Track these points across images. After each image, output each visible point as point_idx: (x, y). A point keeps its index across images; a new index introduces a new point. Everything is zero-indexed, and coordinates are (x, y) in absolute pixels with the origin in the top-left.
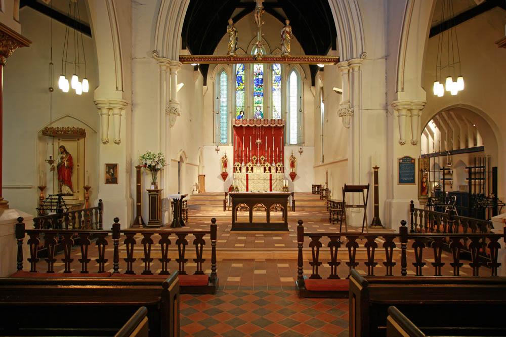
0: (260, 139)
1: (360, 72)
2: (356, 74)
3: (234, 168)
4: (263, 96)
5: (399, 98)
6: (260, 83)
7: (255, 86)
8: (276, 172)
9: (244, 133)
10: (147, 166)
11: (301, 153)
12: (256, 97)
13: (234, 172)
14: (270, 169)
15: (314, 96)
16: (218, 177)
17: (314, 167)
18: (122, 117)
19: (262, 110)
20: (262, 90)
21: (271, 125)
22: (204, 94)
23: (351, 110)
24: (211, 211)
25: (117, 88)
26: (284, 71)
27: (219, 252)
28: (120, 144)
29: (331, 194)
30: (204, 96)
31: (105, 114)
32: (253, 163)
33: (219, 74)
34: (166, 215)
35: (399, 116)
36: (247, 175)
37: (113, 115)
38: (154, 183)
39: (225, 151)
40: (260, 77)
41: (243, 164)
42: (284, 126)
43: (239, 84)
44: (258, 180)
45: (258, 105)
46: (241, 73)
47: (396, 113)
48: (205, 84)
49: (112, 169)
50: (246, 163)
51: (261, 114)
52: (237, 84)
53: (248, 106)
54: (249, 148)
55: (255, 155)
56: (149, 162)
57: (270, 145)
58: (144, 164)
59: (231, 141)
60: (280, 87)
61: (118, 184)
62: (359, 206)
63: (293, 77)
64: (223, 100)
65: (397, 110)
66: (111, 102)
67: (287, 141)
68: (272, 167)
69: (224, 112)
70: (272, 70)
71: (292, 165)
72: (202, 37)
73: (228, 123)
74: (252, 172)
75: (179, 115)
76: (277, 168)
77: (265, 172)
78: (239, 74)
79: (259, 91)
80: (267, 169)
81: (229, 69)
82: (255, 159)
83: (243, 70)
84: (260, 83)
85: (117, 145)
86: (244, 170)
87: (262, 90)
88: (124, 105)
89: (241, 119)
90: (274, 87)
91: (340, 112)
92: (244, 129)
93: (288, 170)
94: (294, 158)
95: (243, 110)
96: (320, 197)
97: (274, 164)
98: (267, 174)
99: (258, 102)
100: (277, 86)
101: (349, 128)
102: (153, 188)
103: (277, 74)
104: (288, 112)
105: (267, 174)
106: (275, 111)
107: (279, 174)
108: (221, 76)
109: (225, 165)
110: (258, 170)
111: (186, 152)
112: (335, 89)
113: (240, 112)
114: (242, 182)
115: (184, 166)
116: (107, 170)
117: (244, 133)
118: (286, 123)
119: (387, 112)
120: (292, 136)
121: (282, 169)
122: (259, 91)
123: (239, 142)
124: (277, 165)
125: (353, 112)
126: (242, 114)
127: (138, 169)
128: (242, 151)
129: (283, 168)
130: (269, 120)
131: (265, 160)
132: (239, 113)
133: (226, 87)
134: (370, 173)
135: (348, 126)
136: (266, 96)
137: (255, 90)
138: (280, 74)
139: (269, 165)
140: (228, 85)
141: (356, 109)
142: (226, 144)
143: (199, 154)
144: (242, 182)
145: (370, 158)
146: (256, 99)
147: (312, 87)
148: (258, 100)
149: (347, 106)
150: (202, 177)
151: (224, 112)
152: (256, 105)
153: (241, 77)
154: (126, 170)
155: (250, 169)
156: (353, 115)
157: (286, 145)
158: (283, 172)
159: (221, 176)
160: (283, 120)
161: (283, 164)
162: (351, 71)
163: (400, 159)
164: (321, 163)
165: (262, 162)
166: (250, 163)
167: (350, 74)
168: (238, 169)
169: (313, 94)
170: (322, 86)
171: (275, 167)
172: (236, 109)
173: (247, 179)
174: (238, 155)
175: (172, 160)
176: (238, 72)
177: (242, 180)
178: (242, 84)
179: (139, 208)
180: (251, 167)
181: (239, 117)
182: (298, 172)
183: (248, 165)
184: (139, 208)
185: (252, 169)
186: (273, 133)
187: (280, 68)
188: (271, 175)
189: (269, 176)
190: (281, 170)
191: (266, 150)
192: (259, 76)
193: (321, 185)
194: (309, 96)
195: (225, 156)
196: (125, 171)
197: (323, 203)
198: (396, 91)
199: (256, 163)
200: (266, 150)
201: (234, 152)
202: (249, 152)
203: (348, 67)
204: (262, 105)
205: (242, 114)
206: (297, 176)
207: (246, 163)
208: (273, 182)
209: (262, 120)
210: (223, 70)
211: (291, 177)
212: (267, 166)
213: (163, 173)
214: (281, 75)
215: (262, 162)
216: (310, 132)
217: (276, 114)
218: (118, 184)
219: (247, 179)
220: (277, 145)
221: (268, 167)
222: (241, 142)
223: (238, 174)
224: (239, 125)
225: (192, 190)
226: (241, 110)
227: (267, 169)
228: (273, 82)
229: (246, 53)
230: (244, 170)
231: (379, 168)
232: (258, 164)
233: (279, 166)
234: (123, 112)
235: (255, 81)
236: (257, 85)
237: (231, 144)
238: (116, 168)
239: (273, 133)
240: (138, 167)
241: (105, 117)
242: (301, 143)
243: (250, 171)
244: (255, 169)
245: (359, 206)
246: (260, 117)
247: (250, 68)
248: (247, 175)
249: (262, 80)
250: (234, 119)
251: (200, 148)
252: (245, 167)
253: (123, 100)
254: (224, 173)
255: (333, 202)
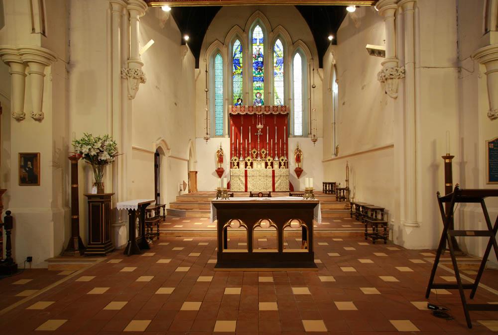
0: (259, 129)
1: (417, 10)
2: (409, 14)
3: (231, 163)
4: (263, 81)
5: (492, 42)
6: (260, 66)
7: (254, 70)
8: (280, 168)
9: (242, 123)
10: (83, 155)
11: (315, 142)
12: (255, 82)
13: (231, 168)
14: (272, 164)
15: (322, 80)
16: (212, 174)
17: (323, 162)
18: (45, 78)
19: (262, 97)
20: (262, 75)
21: (274, 113)
22: (195, 77)
23: (401, 70)
24: (197, 219)
25: (33, 29)
26: (286, 52)
27: (230, 232)
28: (43, 121)
29: (351, 195)
30: (196, 81)
31: (18, 73)
32: (252, 158)
33: (214, 57)
34: (120, 233)
35: (487, 74)
36: (246, 171)
37: (30, 74)
38: (99, 184)
39: (221, 143)
40: (260, 59)
41: (241, 159)
42: (288, 113)
43: (236, 67)
44: (257, 179)
45: (258, 91)
46: (239, 56)
47: (483, 69)
48: (197, 66)
49: (30, 161)
50: (244, 158)
51: (261, 101)
52: (234, 68)
53: (246, 92)
54: (248, 141)
55: (255, 148)
56: (85, 150)
57: (272, 137)
58: (78, 152)
59: (227, 133)
60: (282, 70)
61: (39, 185)
62: (478, 233)
63: (298, 58)
64: (220, 90)
65: (484, 64)
66: (22, 51)
67: (291, 132)
68: (274, 162)
69: (219, 100)
70: (273, 51)
71: (298, 159)
72: (195, 26)
73: (224, 112)
74: (252, 168)
75: (143, 80)
76: (280, 163)
77: (266, 168)
78: (236, 56)
79: (258, 76)
80: (269, 164)
81: (224, 50)
82: (254, 152)
83: (241, 52)
84: (260, 66)
85: (37, 122)
86: (242, 165)
87: (262, 75)
88: (49, 59)
89: (239, 106)
90: (275, 71)
91: (383, 74)
92: (242, 119)
93: (293, 165)
94: (300, 151)
95: (241, 98)
96: (337, 198)
97: (277, 159)
98: (269, 170)
99: (259, 88)
100: (279, 70)
101: (396, 98)
102: (94, 191)
103: (278, 57)
104: (291, 97)
105: (269, 170)
106: (277, 98)
107: (283, 170)
108: (216, 60)
109: (221, 159)
110: (259, 166)
111: (165, 140)
112: (368, 46)
113: (238, 100)
114: (240, 179)
115: (165, 161)
116: (22, 164)
117: (242, 123)
118: (289, 110)
119: (459, 72)
120: (297, 127)
121: (286, 165)
122: (258, 76)
123: (237, 134)
124: (281, 159)
125: (404, 73)
126: (240, 102)
127: (74, 162)
128: (240, 144)
129: (288, 162)
130: (271, 106)
131: (266, 153)
132: (236, 100)
133: (221, 71)
134: (435, 167)
135: (395, 96)
136: (267, 80)
137: (254, 75)
138: (282, 56)
139: (272, 159)
140: (223, 70)
141: (409, 68)
142: (223, 136)
143: (189, 145)
144: (240, 179)
145: (434, 144)
146: (256, 84)
147: (320, 70)
148: (257, 85)
149: (393, 64)
150: (193, 175)
151: (219, 100)
152: (255, 91)
153: (238, 60)
154: (54, 162)
155: (249, 164)
156: (405, 77)
157: (290, 136)
158: (288, 168)
159: (216, 173)
160: (287, 106)
161: (287, 158)
162: (400, 10)
163: (489, 143)
164: (333, 157)
165: (263, 156)
166: (249, 158)
167: (399, 17)
168: (236, 164)
169: (321, 77)
170: (334, 62)
171: (278, 162)
172: (233, 96)
173: (246, 176)
174: (235, 148)
175: (134, 148)
176: (235, 54)
177: (240, 177)
178: (239, 68)
179: (75, 224)
180: (250, 161)
181: (236, 105)
182: (305, 168)
183: (247, 159)
184: (75, 224)
185: (252, 164)
186: (275, 123)
187: (282, 49)
188: (273, 172)
189: (271, 172)
190: (284, 165)
191: (268, 142)
192: (259, 59)
193: (335, 183)
194: (317, 80)
195: (221, 149)
196: (51, 164)
197: (340, 206)
198: (483, 31)
199: (256, 157)
200: (268, 142)
201: (231, 144)
202: (248, 144)
203: (395, 6)
204: (262, 91)
205: (240, 102)
206: (303, 172)
207: (244, 158)
208: (276, 179)
209: (263, 106)
210: (218, 52)
211: (297, 174)
212: (269, 160)
213: (116, 168)
214: (284, 57)
215: (263, 156)
216: (318, 121)
217: (279, 100)
218: (39, 185)
219: (246, 176)
220: (281, 136)
221: (270, 161)
222: (238, 134)
223: (236, 170)
224: (236, 113)
225: (179, 190)
226: (238, 98)
227: (269, 164)
228: (275, 65)
229: (244, 31)
230: (242, 165)
231: (452, 157)
232: (259, 159)
233: (282, 160)
234: (48, 70)
235: (254, 65)
236: (257, 69)
237: (227, 136)
238: (36, 161)
239: (275, 123)
240: (75, 159)
241: (17, 79)
242: (307, 133)
243: (249, 166)
244: (255, 164)
245: (478, 233)
246: (260, 104)
247: (248, 49)
248: (246, 171)
249: (262, 63)
250: (230, 106)
251: (190, 140)
252: (244, 162)
253: (43, 49)
254: (219, 169)
255: (357, 205)
